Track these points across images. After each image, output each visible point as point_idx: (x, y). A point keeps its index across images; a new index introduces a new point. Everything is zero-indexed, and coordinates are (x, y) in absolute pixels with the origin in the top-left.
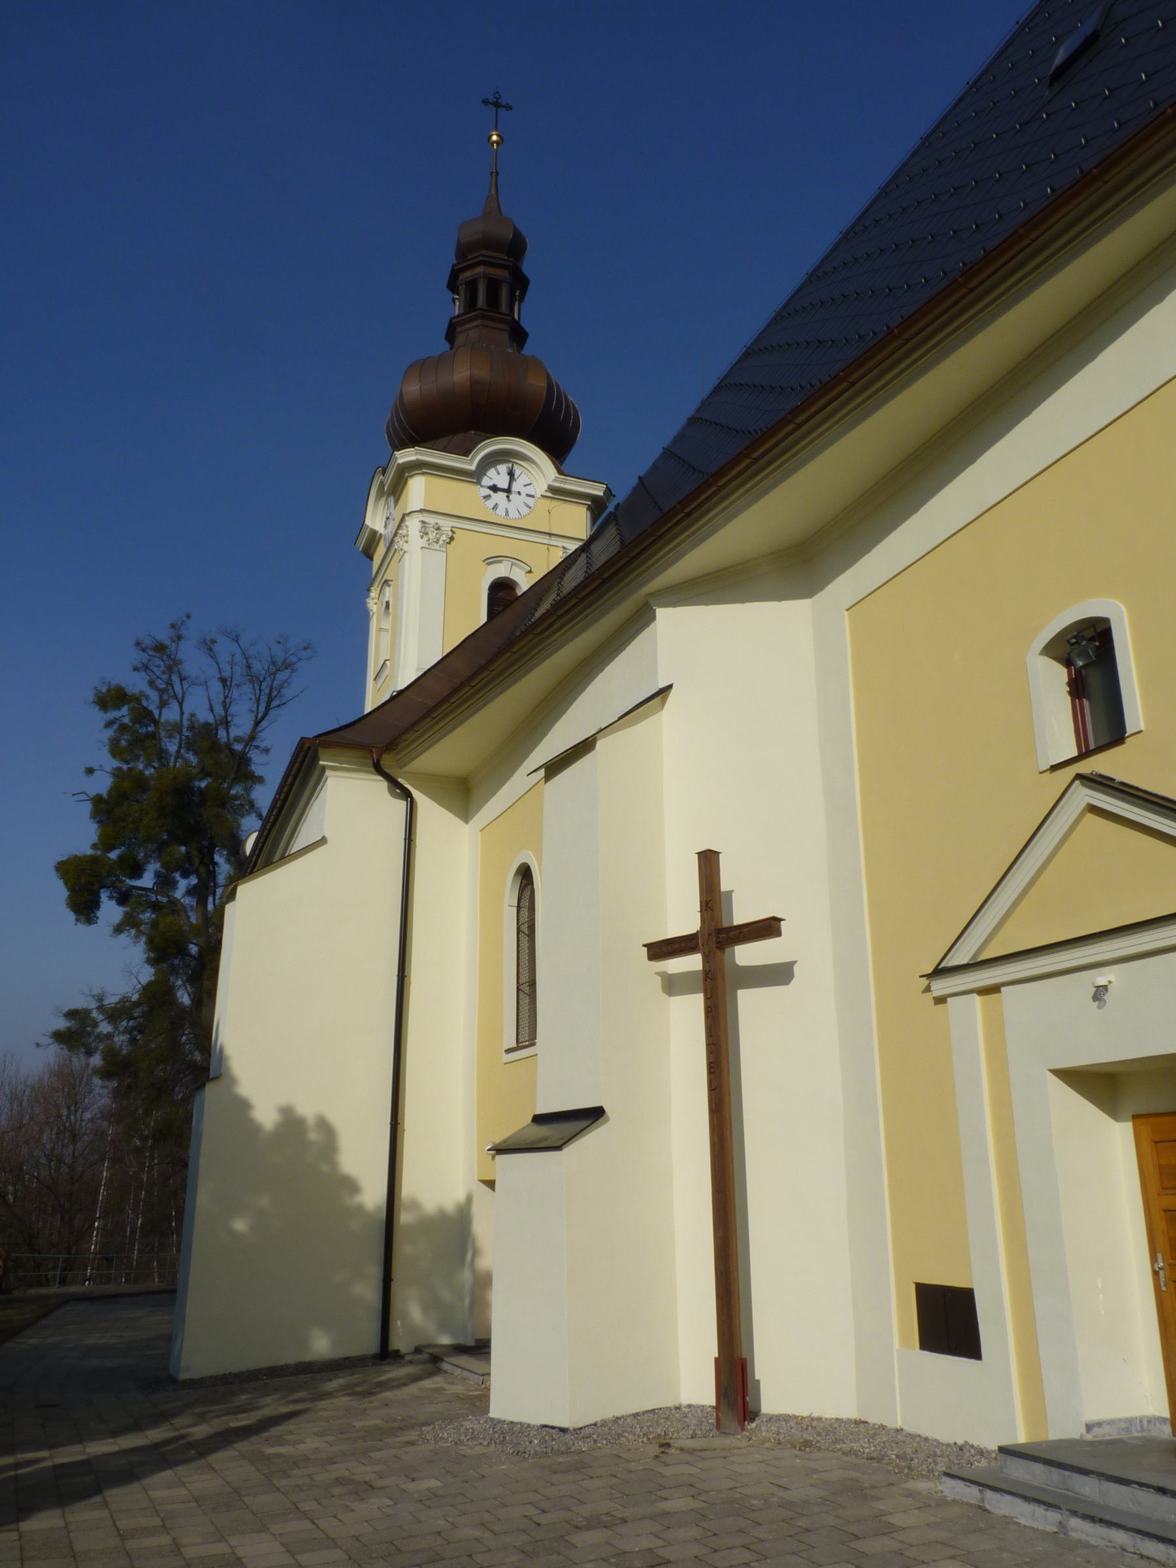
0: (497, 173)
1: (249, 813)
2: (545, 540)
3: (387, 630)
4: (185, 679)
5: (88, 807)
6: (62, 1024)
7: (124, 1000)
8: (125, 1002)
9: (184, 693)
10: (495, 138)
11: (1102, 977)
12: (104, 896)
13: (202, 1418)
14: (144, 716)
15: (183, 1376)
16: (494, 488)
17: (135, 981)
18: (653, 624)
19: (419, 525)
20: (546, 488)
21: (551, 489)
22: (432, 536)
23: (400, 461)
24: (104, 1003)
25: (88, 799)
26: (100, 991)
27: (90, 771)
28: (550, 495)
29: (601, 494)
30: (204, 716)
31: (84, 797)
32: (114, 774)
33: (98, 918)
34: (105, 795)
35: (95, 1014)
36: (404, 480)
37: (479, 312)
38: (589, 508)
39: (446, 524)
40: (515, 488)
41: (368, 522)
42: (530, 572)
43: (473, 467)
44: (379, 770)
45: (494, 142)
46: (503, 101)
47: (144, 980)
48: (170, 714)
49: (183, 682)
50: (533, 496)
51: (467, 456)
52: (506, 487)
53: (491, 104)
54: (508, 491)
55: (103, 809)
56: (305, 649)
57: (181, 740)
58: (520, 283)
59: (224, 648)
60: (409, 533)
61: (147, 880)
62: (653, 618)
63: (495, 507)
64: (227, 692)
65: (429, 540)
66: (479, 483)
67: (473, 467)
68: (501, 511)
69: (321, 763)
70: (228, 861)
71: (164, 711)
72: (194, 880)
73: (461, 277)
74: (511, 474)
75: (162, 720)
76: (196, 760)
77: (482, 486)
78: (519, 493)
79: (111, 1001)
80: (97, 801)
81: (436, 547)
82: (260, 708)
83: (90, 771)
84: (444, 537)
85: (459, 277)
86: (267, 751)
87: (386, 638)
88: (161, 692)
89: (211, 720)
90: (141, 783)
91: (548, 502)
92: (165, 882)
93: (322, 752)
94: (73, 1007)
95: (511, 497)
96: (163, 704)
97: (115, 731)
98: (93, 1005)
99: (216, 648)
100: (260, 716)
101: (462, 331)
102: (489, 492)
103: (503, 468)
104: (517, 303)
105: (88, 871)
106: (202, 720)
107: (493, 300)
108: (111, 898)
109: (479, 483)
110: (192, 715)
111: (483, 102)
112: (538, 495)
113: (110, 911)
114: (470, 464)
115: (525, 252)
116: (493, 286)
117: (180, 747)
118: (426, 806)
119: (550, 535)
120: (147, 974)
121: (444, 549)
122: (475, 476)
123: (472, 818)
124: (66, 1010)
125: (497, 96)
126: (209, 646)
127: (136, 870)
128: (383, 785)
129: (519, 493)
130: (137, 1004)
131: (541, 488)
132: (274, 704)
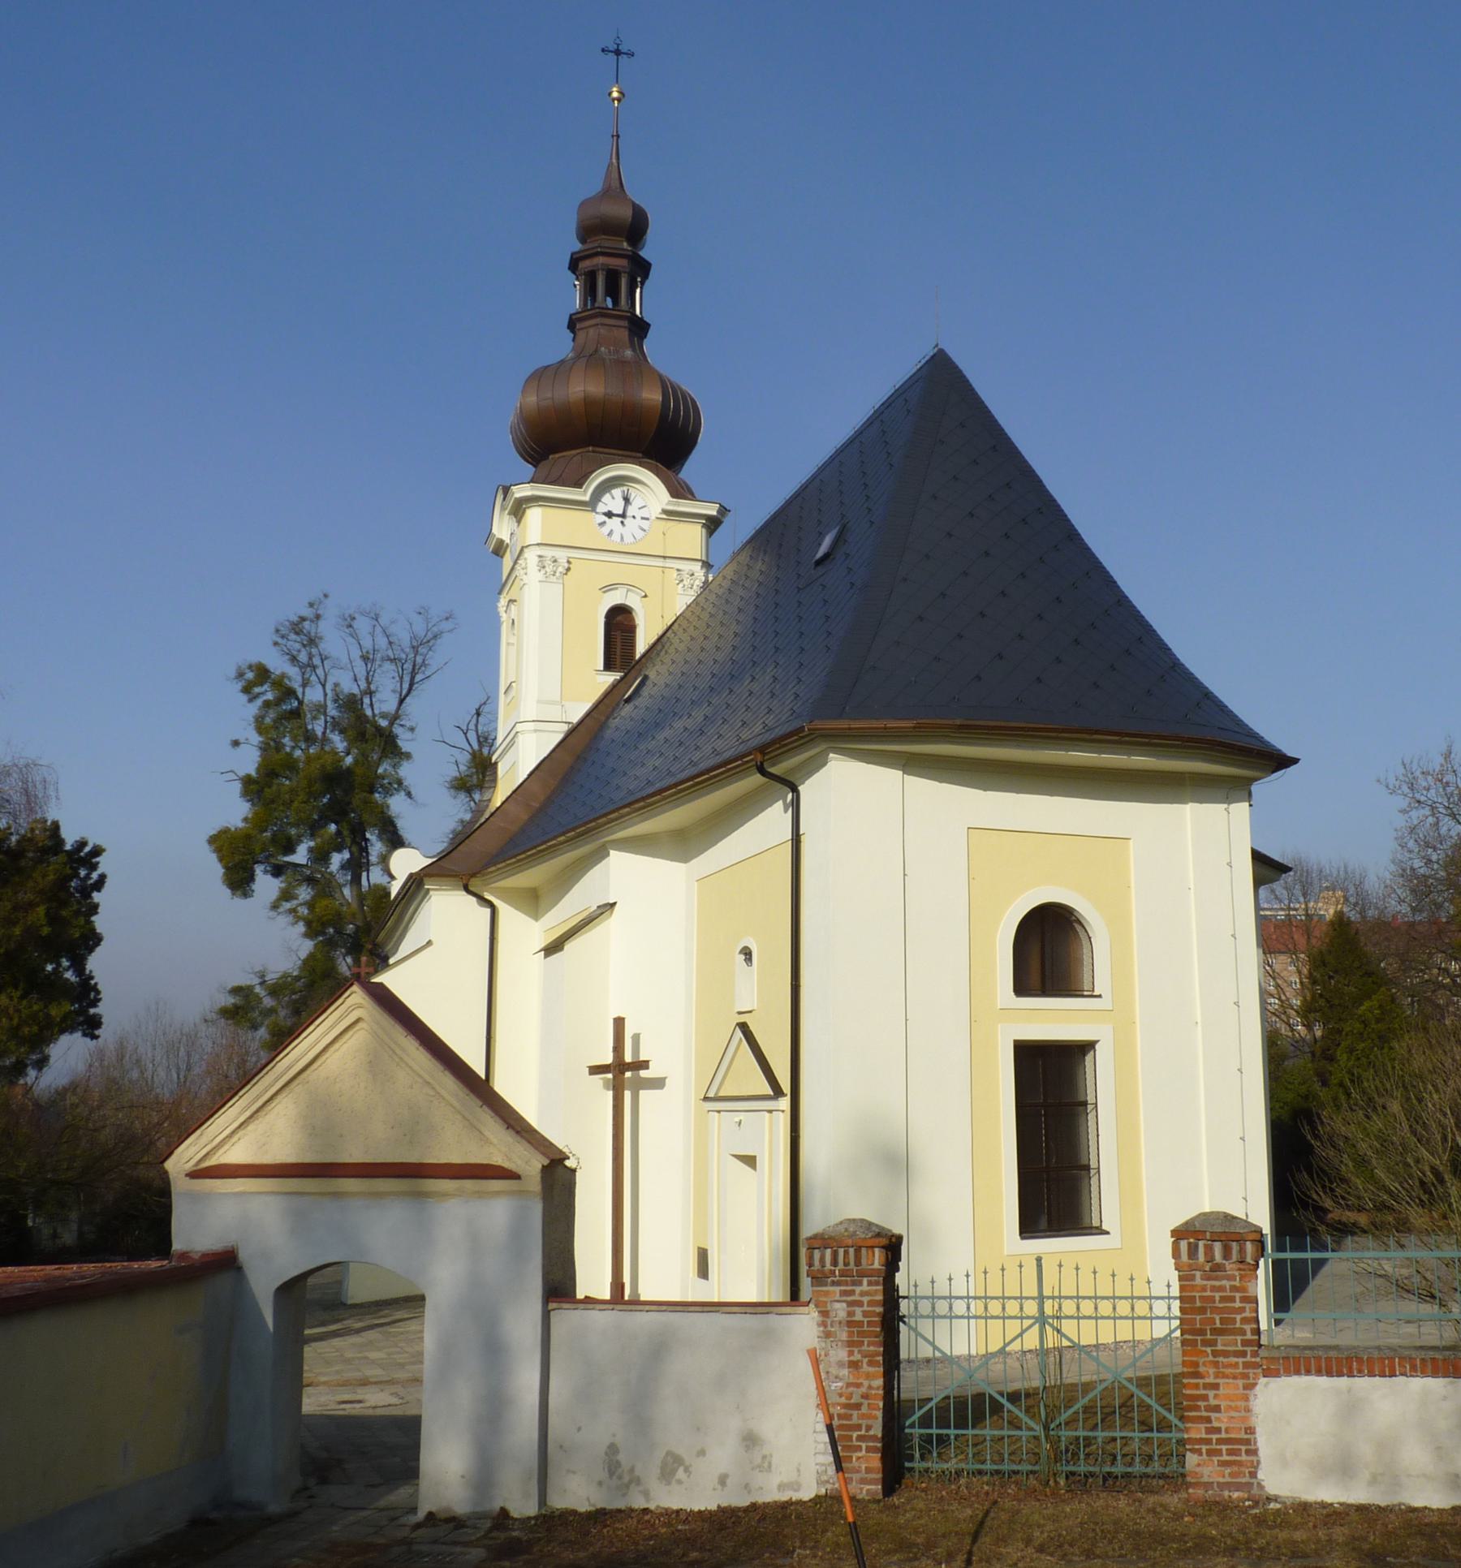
0: (618, 136)
1: (397, 790)
2: (659, 562)
3: (513, 644)
4: (326, 658)
5: (237, 787)
6: (231, 1001)
7: (285, 976)
8: (287, 978)
9: (326, 676)
10: (615, 95)
11: (742, 1116)
12: (259, 869)
13: (360, 1320)
14: (287, 693)
15: (350, 1302)
16: (609, 515)
17: (295, 958)
18: (607, 859)
19: (537, 559)
20: (660, 511)
21: (665, 512)
22: (549, 569)
23: (517, 495)
24: (266, 979)
25: (236, 778)
26: (261, 968)
27: (236, 743)
28: (664, 516)
29: (715, 513)
30: (349, 687)
31: (232, 776)
32: (261, 748)
33: (253, 891)
34: (253, 774)
35: (258, 989)
36: (422, 893)
37: (597, 310)
38: (704, 525)
39: (562, 555)
40: (630, 513)
41: (495, 531)
42: (646, 596)
43: (587, 498)
44: (467, 889)
45: (614, 100)
46: (623, 48)
47: (303, 955)
48: (313, 695)
49: (325, 662)
50: (647, 519)
51: (581, 488)
52: (621, 512)
53: (612, 52)
54: (623, 516)
55: (253, 788)
56: (447, 619)
57: (326, 722)
58: (641, 269)
59: (363, 625)
60: (528, 565)
61: (301, 856)
62: (608, 855)
63: (610, 534)
64: (369, 666)
65: (546, 572)
66: (594, 510)
67: (587, 498)
68: (616, 537)
69: (426, 887)
70: (380, 838)
71: (308, 690)
72: (346, 855)
73: (580, 266)
74: (627, 500)
75: (306, 701)
76: (345, 744)
77: (597, 513)
78: (634, 517)
79: (271, 977)
80: (247, 781)
81: (554, 579)
82: (404, 686)
83: (236, 743)
84: (561, 569)
85: (578, 266)
86: (412, 729)
87: (513, 650)
88: (303, 667)
89: (356, 691)
90: (290, 765)
91: (663, 522)
92: (321, 856)
93: (426, 880)
94: (236, 984)
95: (626, 521)
96: (305, 684)
97: (260, 709)
98: (257, 981)
99: (355, 624)
100: (404, 692)
101: (582, 329)
102: (605, 518)
103: (617, 492)
104: (638, 291)
105: (242, 850)
106: (346, 691)
107: (613, 291)
108: (265, 872)
109: (594, 510)
110: (336, 685)
111: (603, 50)
112: (653, 518)
113: (266, 885)
114: (584, 494)
115: (646, 231)
116: (613, 277)
117: (325, 728)
118: (504, 909)
119: (664, 557)
120: (307, 947)
121: (561, 581)
122: (591, 505)
123: (543, 916)
124: (229, 987)
125: (618, 41)
126: (349, 623)
127: (290, 849)
128: (474, 899)
129: (634, 517)
130: (297, 978)
131: (655, 510)
132: (418, 678)
